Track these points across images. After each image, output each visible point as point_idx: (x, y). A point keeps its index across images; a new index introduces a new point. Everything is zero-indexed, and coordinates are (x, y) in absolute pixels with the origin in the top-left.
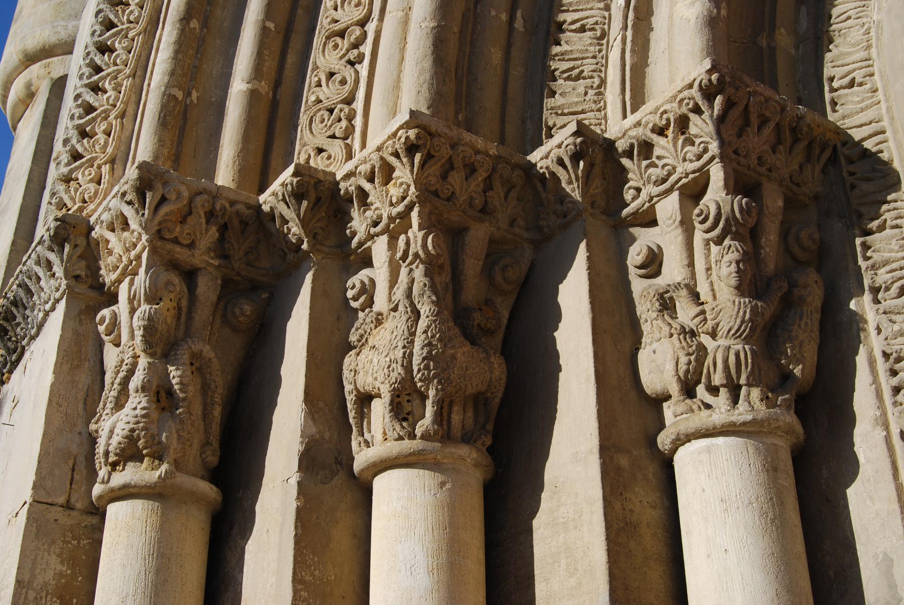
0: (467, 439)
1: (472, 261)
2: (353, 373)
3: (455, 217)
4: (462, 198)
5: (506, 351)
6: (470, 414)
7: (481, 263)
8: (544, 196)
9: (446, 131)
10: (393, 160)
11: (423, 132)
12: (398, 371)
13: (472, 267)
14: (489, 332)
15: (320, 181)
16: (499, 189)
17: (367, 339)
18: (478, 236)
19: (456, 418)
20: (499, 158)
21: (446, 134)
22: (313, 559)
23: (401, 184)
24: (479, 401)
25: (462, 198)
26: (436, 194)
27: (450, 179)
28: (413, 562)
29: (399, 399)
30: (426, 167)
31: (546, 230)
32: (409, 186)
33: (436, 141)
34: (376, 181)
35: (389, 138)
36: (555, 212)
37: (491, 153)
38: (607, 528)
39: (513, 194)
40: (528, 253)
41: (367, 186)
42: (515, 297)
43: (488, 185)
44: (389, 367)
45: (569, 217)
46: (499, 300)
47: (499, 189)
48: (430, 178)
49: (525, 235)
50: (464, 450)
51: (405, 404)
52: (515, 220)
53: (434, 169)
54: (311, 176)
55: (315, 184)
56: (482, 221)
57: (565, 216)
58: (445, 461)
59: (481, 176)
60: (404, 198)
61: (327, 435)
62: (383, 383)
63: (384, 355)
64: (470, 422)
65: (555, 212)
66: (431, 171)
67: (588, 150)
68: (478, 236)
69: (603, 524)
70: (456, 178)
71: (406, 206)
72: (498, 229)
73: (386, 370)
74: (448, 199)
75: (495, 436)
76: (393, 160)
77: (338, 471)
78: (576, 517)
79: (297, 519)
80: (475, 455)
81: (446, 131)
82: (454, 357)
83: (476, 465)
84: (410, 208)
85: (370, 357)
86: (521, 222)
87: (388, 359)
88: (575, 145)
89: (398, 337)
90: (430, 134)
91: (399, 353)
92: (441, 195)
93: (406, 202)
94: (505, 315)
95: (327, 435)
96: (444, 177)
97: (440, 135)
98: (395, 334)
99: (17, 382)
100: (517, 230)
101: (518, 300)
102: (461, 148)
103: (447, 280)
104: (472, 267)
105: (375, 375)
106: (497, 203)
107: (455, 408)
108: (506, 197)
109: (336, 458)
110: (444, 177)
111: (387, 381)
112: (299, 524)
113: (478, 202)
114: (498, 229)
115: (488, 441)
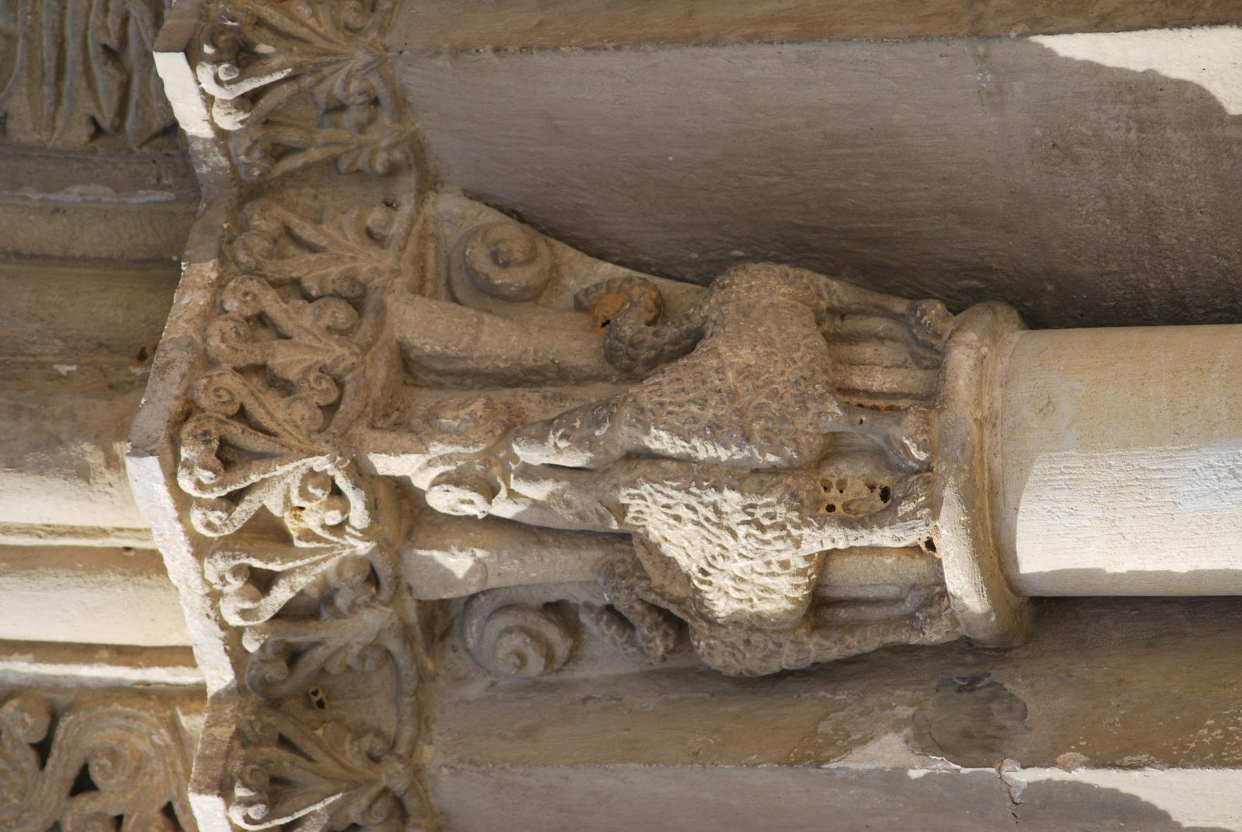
0: (931, 357)
1: (484, 338)
2: (756, 638)
3: (380, 371)
4: (337, 353)
5: (706, 276)
6: (867, 351)
7: (487, 318)
8: (315, 154)
9: (175, 374)
10: (244, 512)
11: (189, 427)
12: (771, 504)
13: (500, 340)
14: (661, 312)
15: (238, 734)
16: (298, 265)
17: (673, 602)
18: (421, 324)
19: (880, 381)
20: (224, 259)
21: (183, 376)
22: (1211, 729)
23: (304, 493)
24: (837, 331)
25: (337, 353)
26: (330, 410)
27: (293, 374)
28: (1224, 473)
29: (838, 506)
30: (271, 426)
31: (397, 155)
32: (312, 473)
33: (204, 401)
34: (275, 567)
35: (183, 518)
36: (361, 128)
37: (214, 275)
38: (1162, 25)
39: (307, 232)
40: (448, 204)
41: (281, 595)
42: (572, 253)
43: (293, 288)
44: (762, 528)
45: (382, 92)
46: (572, 282)
47: (298, 265)
48: (297, 418)
49: (407, 207)
50: (962, 360)
51: (848, 495)
52: (369, 233)
53: (272, 409)
54: (228, 755)
55: (244, 746)
56: (382, 310)
57: (375, 102)
58: (986, 404)
59: (271, 303)
60: (336, 492)
61: (906, 712)
62: (797, 543)
63: (728, 541)
64: (886, 351)
65: (361, 128)
66: (280, 415)
67: (231, 29)
68: (421, 324)
69: (1154, 32)
70: (287, 360)
71: (356, 486)
72: (396, 272)
73: (768, 536)
74: (340, 384)
75: (917, 294)
76: (244, 512)
77: (991, 684)
78: (1129, 98)
79: (1113, 766)
80: (971, 337)
81: (175, 374)
82: (745, 373)
83: (995, 337)
84: (361, 474)
85: (727, 583)
86: (376, 217)
87: (742, 531)
88: (216, 61)
89: (693, 501)
90: (186, 415)
91: (731, 499)
92: (333, 397)
93: (343, 483)
94: (606, 269)
95: (906, 712)
96: (285, 387)
97: (189, 388)
98: (683, 512)
99: (1182, 813)
100: (397, 229)
101: (576, 244)
102: (214, 342)
103: (535, 396)
104: (500, 340)
105: (776, 568)
106: (335, 271)
107: (857, 381)
108: (313, 249)
109: (960, 690)
110: (285, 387)
111: (795, 532)
112: (1127, 760)
113: (340, 314)
114: (396, 272)
115: (934, 310)
